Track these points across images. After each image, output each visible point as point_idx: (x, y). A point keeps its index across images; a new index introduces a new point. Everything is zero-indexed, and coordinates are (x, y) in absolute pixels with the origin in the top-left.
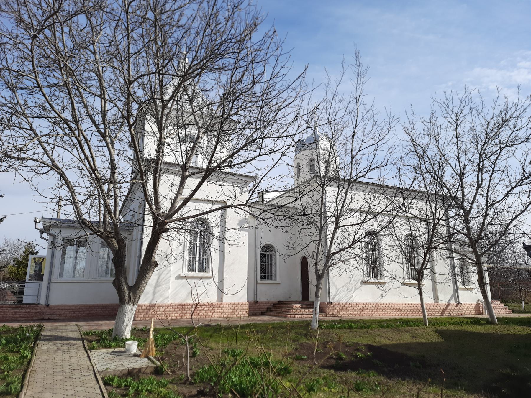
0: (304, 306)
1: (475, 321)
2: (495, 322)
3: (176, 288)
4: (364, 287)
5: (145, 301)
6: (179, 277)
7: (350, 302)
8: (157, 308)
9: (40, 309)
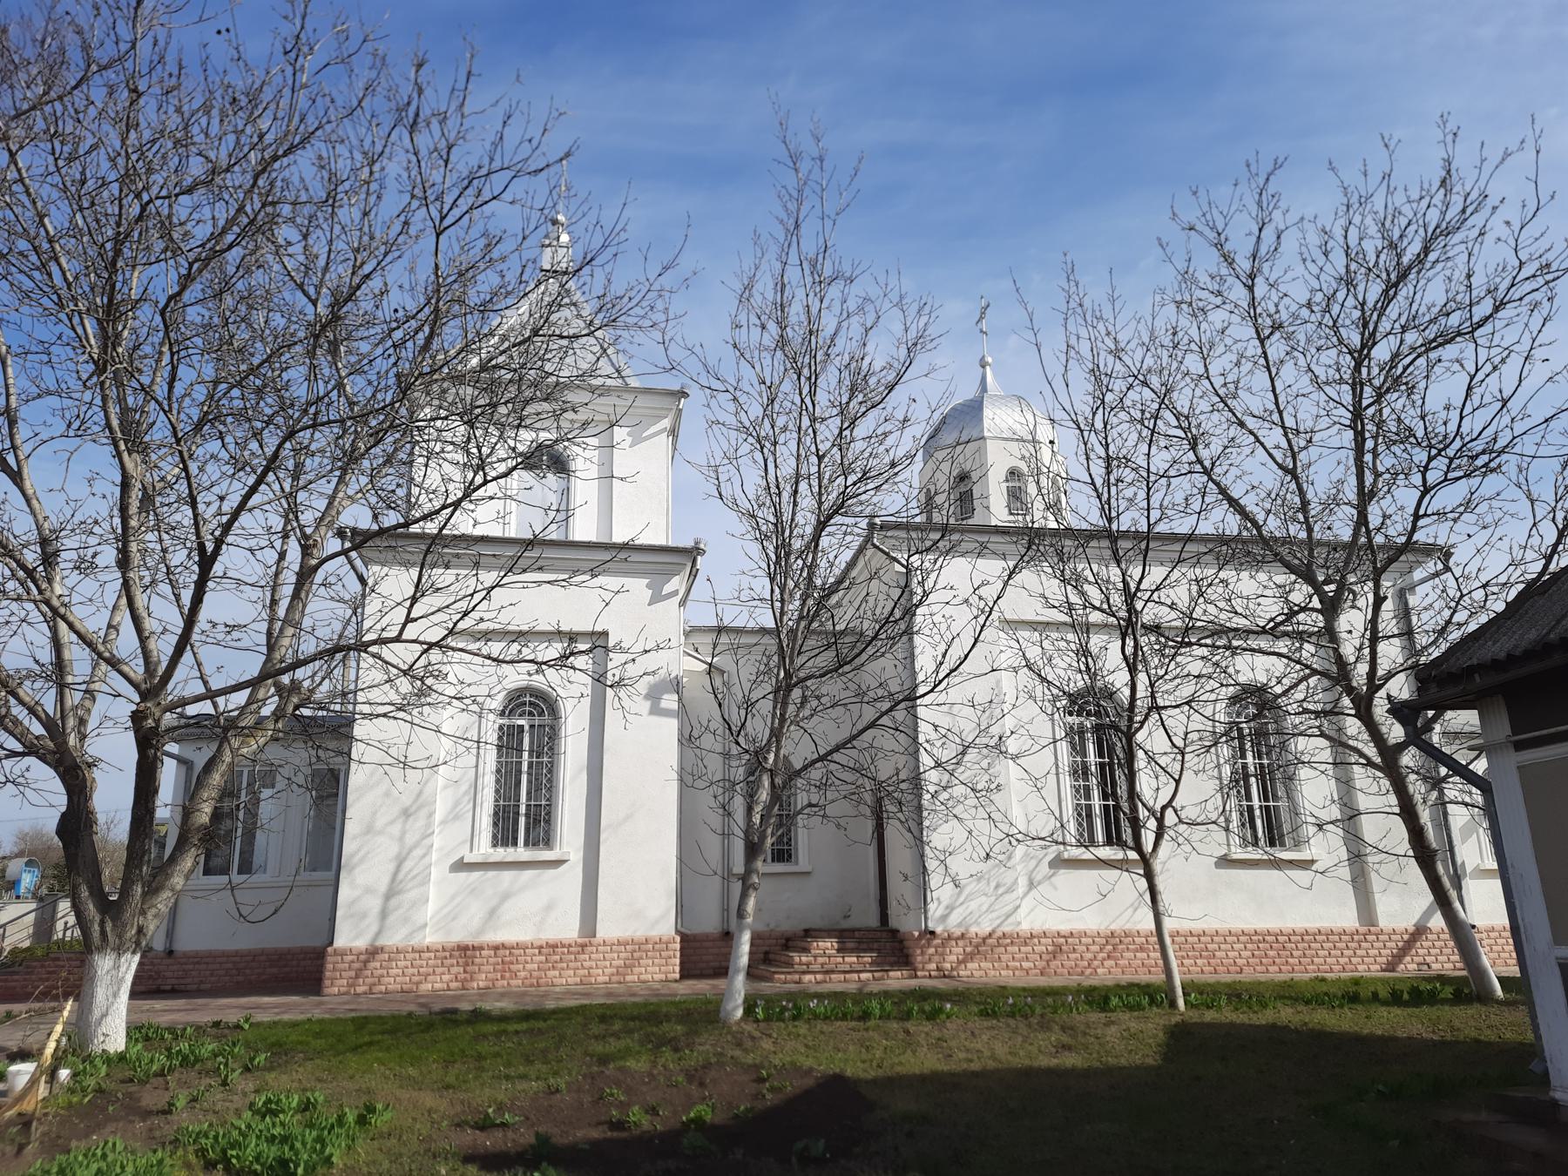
0: (850, 945)
1: (1420, 994)
2: (1492, 991)
3: (453, 898)
4: (1066, 876)
5: (357, 937)
6: (461, 866)
7: (1007, 928)
8: (390, 960)
9: (152, 964)
